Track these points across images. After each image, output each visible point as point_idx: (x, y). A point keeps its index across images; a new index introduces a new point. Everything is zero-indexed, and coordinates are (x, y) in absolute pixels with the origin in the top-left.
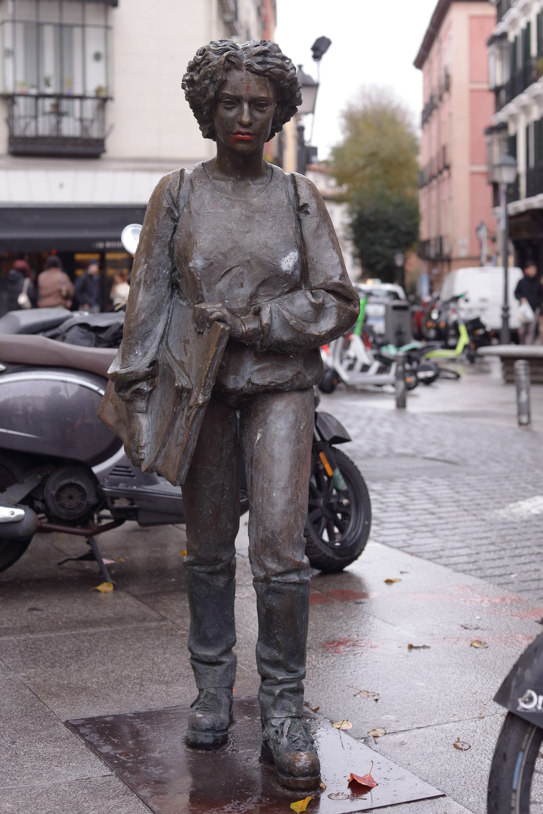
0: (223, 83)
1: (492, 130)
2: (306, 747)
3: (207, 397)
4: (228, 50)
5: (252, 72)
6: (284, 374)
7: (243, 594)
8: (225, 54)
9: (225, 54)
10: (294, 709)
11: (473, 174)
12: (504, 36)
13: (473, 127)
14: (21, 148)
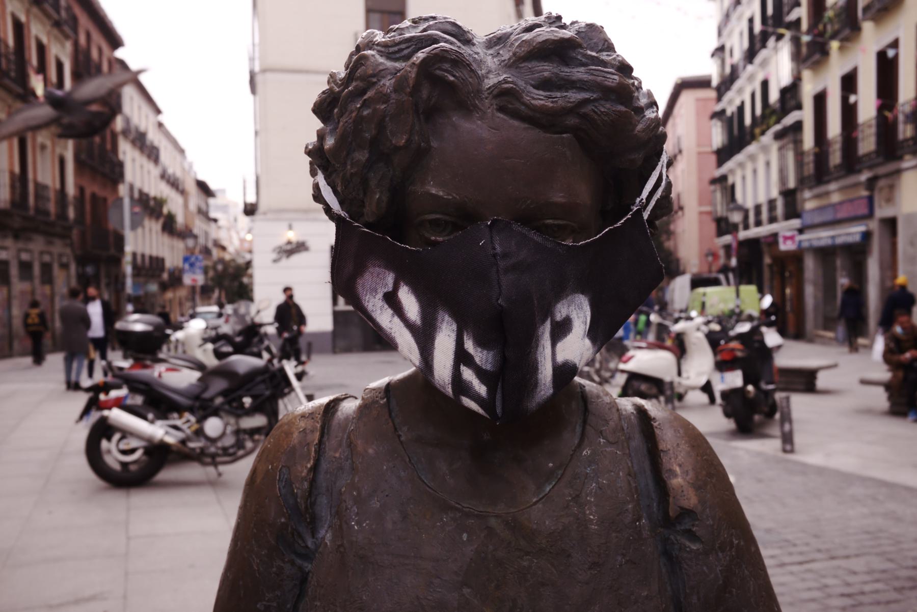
1: (714, 181)
5: (515, 115)
8: (421, 55)
9: (421, 55)
11: (701, 213)
12: (723, 111)
13: (700, 179)
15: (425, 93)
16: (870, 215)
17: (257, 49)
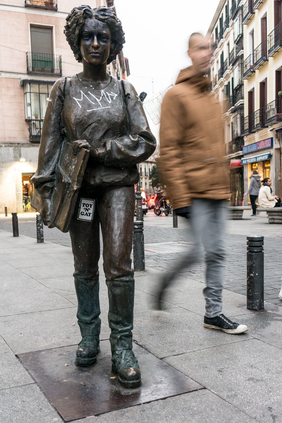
0: (84, 25)
2: (133, 365)
3: (79, 187)
4: (85, 7)
6: (119, 177)
7: (176, 347)
8: (84, 9)
10: (127, 345)
14: (34, 140)
15: (85, 15)
16: (272, 147)
17: (41, 130)
